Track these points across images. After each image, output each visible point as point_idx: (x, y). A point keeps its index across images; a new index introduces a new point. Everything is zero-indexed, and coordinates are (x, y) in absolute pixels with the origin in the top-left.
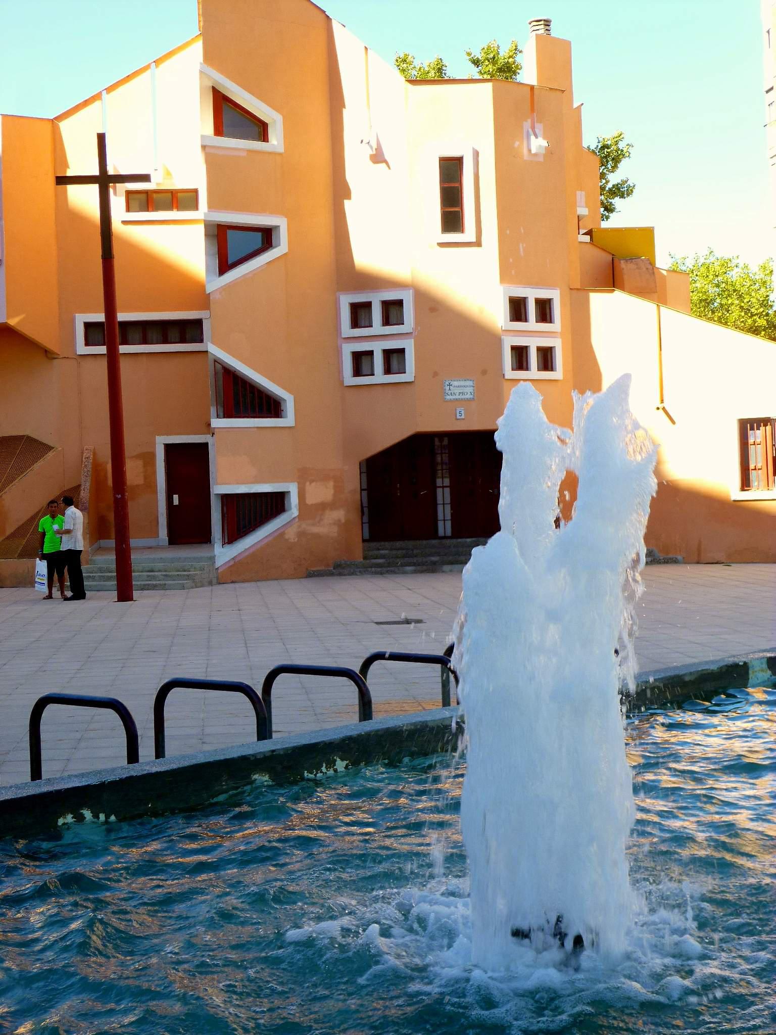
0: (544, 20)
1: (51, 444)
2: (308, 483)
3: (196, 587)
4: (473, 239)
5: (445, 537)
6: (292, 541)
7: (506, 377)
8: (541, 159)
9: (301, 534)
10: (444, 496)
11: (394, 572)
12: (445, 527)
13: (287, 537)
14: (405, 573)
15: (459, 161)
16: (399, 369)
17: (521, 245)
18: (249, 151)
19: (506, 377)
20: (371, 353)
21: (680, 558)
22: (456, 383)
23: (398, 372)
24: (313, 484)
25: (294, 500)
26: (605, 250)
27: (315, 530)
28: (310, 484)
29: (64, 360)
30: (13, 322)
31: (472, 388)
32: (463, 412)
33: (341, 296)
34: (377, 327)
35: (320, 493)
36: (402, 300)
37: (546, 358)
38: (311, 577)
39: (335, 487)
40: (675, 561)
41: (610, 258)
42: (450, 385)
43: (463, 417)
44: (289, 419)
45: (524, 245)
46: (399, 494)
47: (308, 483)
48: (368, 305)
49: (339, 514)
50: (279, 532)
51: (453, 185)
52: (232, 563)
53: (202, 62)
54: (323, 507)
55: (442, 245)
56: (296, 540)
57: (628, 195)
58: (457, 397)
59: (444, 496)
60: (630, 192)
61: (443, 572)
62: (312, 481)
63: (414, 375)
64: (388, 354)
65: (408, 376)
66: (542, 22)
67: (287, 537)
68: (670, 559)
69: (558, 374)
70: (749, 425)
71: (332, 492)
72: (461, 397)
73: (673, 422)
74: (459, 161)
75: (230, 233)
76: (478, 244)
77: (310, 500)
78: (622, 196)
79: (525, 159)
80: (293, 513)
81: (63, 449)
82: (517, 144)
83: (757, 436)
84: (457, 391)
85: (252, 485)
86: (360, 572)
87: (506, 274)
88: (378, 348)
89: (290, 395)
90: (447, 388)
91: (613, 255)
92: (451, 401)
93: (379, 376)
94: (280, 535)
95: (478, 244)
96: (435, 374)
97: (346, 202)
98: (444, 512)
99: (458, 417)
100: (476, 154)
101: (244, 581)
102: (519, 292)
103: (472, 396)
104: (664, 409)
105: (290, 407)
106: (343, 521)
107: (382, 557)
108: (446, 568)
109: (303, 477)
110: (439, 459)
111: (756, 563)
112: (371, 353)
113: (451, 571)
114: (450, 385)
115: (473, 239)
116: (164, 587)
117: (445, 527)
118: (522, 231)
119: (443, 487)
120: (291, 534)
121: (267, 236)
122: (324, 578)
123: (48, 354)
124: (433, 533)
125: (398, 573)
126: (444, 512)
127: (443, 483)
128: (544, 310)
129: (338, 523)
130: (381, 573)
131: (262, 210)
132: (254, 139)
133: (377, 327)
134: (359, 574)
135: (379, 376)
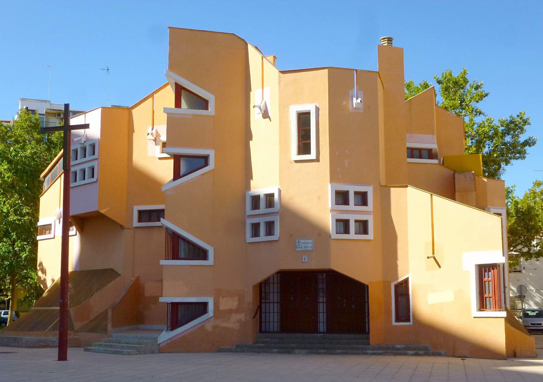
0: (388, 38)
1: (119, 272)
2: (221, 298)
3: (140, 354)
4: (314, 158)
5: (273, 332)
6: (209, 331)
7: (332, 238)
8: (362, 111)
9: (215, 327)
10: (322, 308)
11: (266, 352)
12: (322, 327)
14: (272, 353)
15: (308, 114)
17: (346, 160)
18: (193, 115)
19: (332, 238)
21: (442, 352)
22: (302, 241)
24: (225, 298)
25: (211, 307)
26: (448, 168)
27: (225, 325)
29: (128, 230)
30: (103, 211)
32: (306, 258)
35: (228, 303)
37: (363, 227)
38: (219, 352)
39: (239, 300)
40: (440, 355)
41: (452, 172)
42: (299, 242)
43: (306, 261)
44: (211, 261)
46: (344, 306)
47: (221, 298)
49: (241, 316)
51: (307, 128)
52: (169, 341)
54: (230, 312)
56: (212, 330)
57: (533, 145)
58: (303, 249)
59: (322, 308)
60: (534, 143)
61: (295, 353)
62: (223, 297)
63: (278, 236)
64: (347, 231)
66: (386, 39)
67: (206, 328)
68: (436, 353)
69: (371, 236)
70: (487, 268)
72: (305, 249)
73: (440, 267)
74: (308, 114)
76: (317, 160)
77: (222, 307)
78: (530, 146)
79: (350, 111)
80: (210, 315)
81: (124, 276)
82: (344, 103)
83: (489, 277)
84: (303, 246)
86: (247, 351)
87: (333, 178)
89: (212, 247)
91: (454, 171)
92: (299, 251)
93: (352, 235)
94: (201, 327)
95: (317, 160)
97: (251, 142)
98: (322, 317)
99: (303, 261)
100: (317, 110)
101: (177, 352)
102: (343, 187)
103: (311, 249)
104: (434, 258)
105: (211, 255)
106: (243, 320)
107: (262, 343)
108: (297, 351)
109: (218, 294)
110: (320, 286)
111: (487, 358)
113: (299, 353)
114: (299, 242)
115: (314, 158)
116: (121, 353)
117: (322, 327)
118: (347, 152)
119: (274, 303)
120: (209, 327)
121: (205, 159)
122: (227, 353)
123: (122, 227)
124: (315, 330)
125: (268, 353)
126: (322, 317)
127: (273, 301)
128: (362, 198)
130: (259, 352)
132: (203, 109)
133: (352, 206)
134: (246, 352)
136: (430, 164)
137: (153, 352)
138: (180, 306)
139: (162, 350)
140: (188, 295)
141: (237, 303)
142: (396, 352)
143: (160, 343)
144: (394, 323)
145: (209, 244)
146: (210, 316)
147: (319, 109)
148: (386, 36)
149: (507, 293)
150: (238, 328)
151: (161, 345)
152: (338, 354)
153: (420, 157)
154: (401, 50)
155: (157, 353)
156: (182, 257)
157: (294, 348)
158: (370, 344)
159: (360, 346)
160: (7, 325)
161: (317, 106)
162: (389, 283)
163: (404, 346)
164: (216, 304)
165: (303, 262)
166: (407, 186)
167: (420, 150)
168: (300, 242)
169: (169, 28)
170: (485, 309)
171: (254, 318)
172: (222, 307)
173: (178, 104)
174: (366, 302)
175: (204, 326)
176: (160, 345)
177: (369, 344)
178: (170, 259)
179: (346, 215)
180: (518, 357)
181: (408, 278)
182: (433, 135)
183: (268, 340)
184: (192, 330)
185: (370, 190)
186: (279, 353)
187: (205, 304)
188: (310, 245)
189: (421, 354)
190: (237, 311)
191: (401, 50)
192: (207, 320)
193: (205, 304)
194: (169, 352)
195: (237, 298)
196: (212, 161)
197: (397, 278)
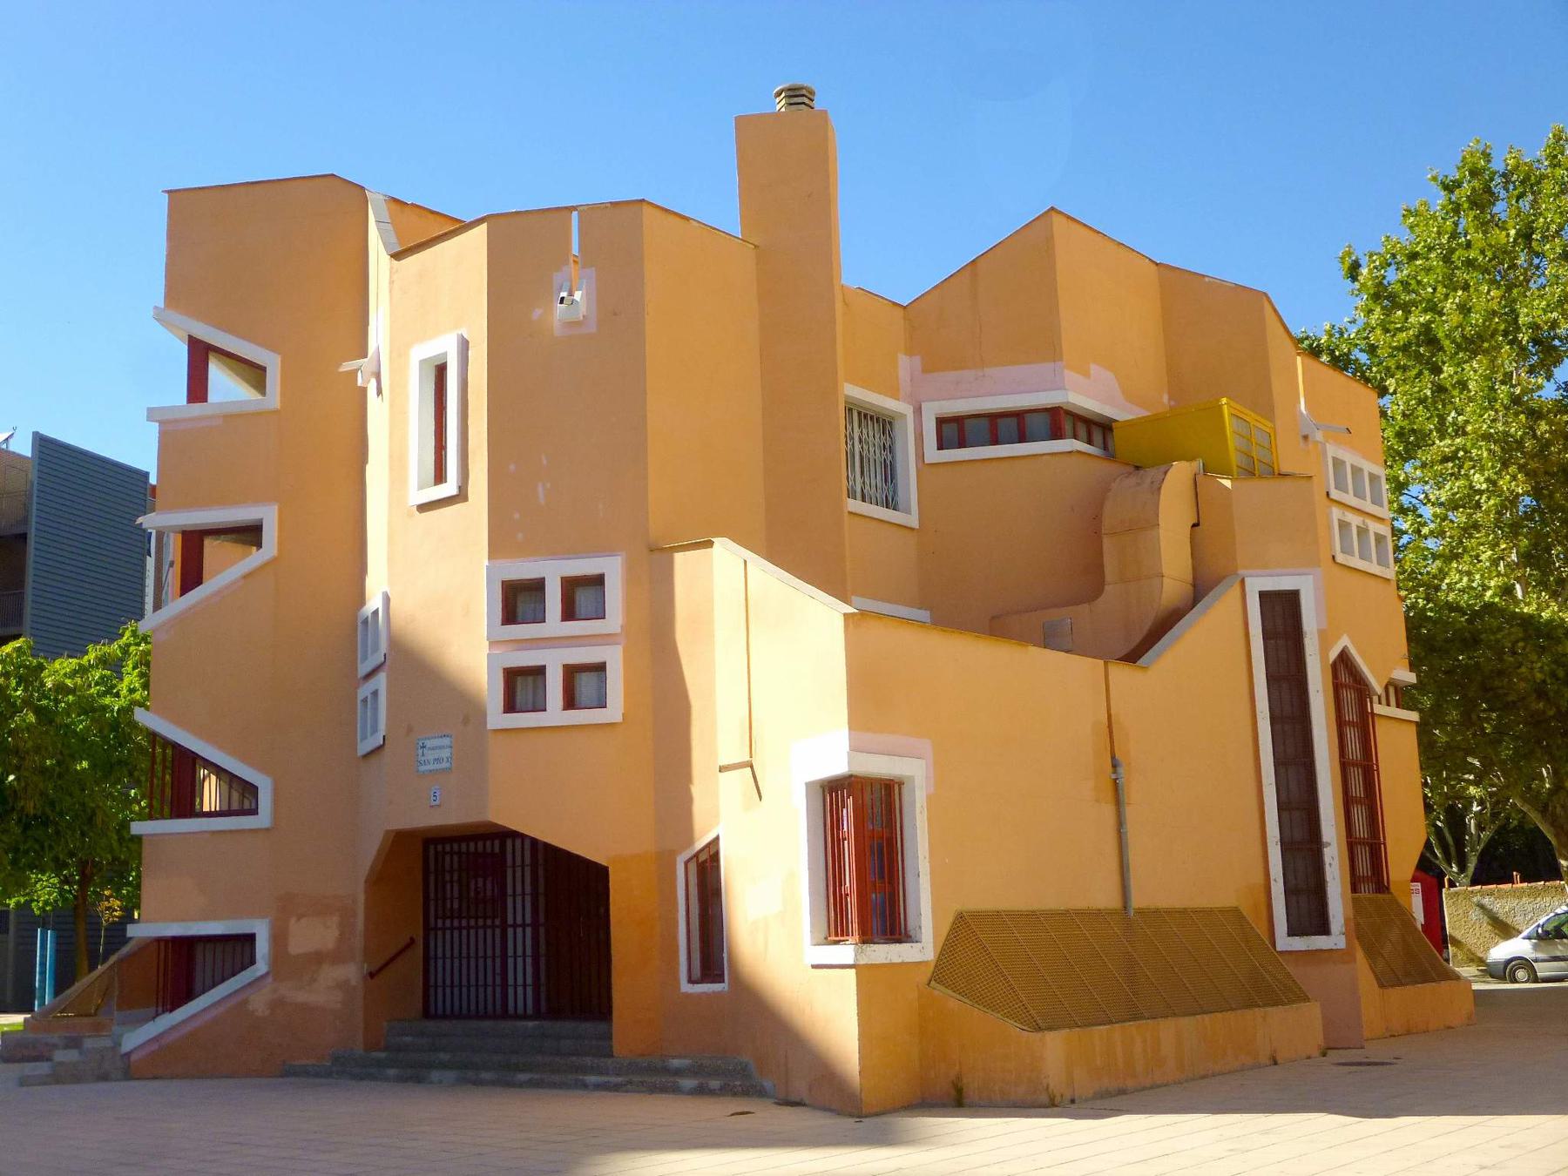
2: (293, 921)
9: (277, 1004)
12: (522, 996)
16: (534, 706)
17: (540, 485)
20: (540, 671)
23: (530, 709)
24: (304, 921)
25: (262, 947)
27: (301, 997)
28: (299, 920)
31: (448, 750)
33: (619, 558)
34: (553, 623)
35: (313, 935)
36: (544, 578)
43: (437, 802)
45: (548, 485)
48: (537, 586)
52: (155, 1047)
53: (162, 305)
54: (318, 959)
55: (423, 508)
61: (431, 1083)
62: (300, 917)
65: (614, 710)
66: (783, 95)
76: (461, 496)
85: (190, 924)
87: (499, 544)
88: (554, 663)
93: (555, 713)
96: (410, 730)
100: (464, 345)
101: (173, 1077)
102: (524, 570)
103: (448, 765)
109: (286, 909)
112: (540, 671)
113: (440, 1082)
118: (545, 462)
120: (259, 1003)
126: (521, 972)
131: (223, 501)
133: (553, 623)
135: (555, 713)
136: (1048, 457)
137: (104, 1077)
138: (199, 949)
139: (130, 1070)
141: (337, 933)
142: (672, 1079)
144: (686, 987)
146: (259, 974)
147: (467, 342)
148: (780, 85)
149: (1330, 864)
150: (339, 1006)
151: (134, 1057)
152: (521, 1085)
153: (1022, 438)
154: (825, 112)
155: (116, 1080)
157: (430, 1066)
158: (614, 1054)
159: (588, 1060)
160: (46, 1003)
164: (279, 939)
166: (709, 544)
167: (1019, 415)
169: (169, 192)
170: (845, 938)
171: (372, 975)
173: (197, 389)
175: (246, 1002)
176: (129, 1058)
177: (612, 1056)
178: (163, 818)
180: (971, 1106)
181: (717, 838)
182: (1054, 361)
183: (408, 1039)
184: (214, 1013)
185: (613, 569)
186: (401, 1079)
189: (715, 1090)
191: (825, 112)
194: (155, 1078)
195: (336, 919)
196: (270, 535)
197: (690, 840)
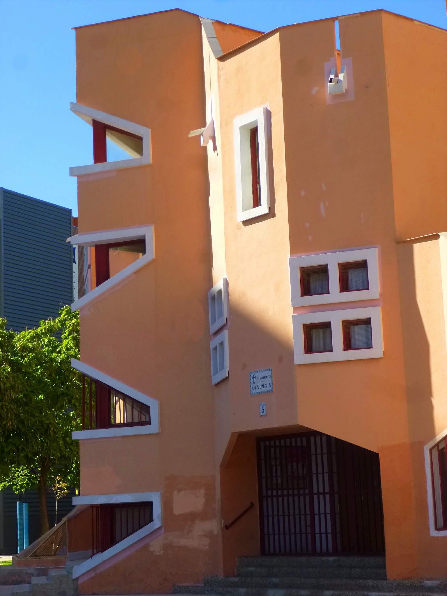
2: (176, 492)
6: (157, 553)
9: (167, 547)
13: (152, 549)
20: (327, 326)
22: (257, 375)
25: (157, 510)
27: (183, 542)
31: (270, 378)
32: (264, 408)
33: (377, 249)
47: (176, 492)
48: (323, 270)
50: (142, 544)
56: (162, 552)
62: (179, 491)
67: (152, 549)
71: (203, 500)
72: (263, 390)
75: (113, 253)
76: (271, 214)
77: (178, 510)
82: (315, 90)
90: (252, 381)
99: (262, 414)
100: (268, 115)
103: (270, 388)
112: (327, 326)
114: (254, 377)
129: (209, 535)
140: (120, 491)
143: (78, 578)
144: (434, 533)
145: (150, 395)
151: (80, 582)
156: (118, 422)
159: (370, 582)
161: (269, 109)
162: (422, 444)
163: (438, 582)
164: (167, 505)
165: (261, 416)
166: (437, 237)
168: (255, 377)
172: (178, 510)
174: (327, 493)
175: (146, 547)
176: (77, 581)
177: (386, 579)
179: (322, 313)
183: (252, 569)
187: (149, 505)
188: (42, 397)
190: (204, 516)
192: (151, 533)
193: (149, 505)
195: (202, 492)
196: (150, 245)
